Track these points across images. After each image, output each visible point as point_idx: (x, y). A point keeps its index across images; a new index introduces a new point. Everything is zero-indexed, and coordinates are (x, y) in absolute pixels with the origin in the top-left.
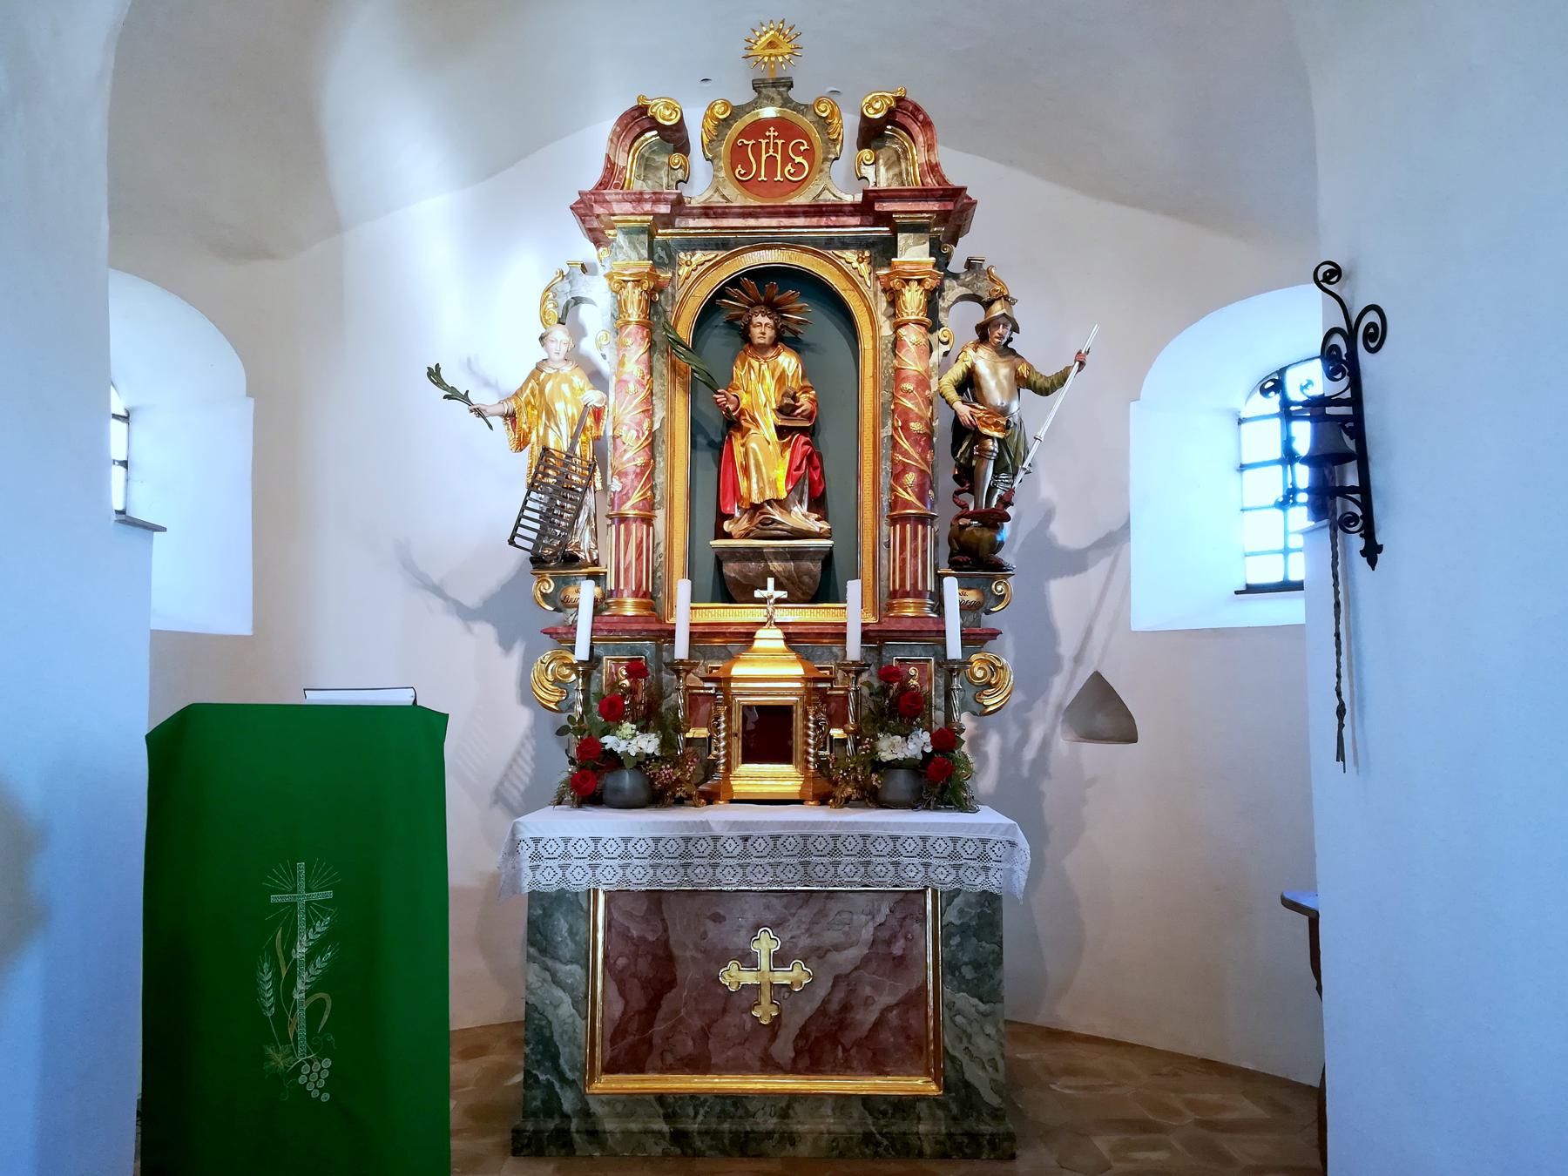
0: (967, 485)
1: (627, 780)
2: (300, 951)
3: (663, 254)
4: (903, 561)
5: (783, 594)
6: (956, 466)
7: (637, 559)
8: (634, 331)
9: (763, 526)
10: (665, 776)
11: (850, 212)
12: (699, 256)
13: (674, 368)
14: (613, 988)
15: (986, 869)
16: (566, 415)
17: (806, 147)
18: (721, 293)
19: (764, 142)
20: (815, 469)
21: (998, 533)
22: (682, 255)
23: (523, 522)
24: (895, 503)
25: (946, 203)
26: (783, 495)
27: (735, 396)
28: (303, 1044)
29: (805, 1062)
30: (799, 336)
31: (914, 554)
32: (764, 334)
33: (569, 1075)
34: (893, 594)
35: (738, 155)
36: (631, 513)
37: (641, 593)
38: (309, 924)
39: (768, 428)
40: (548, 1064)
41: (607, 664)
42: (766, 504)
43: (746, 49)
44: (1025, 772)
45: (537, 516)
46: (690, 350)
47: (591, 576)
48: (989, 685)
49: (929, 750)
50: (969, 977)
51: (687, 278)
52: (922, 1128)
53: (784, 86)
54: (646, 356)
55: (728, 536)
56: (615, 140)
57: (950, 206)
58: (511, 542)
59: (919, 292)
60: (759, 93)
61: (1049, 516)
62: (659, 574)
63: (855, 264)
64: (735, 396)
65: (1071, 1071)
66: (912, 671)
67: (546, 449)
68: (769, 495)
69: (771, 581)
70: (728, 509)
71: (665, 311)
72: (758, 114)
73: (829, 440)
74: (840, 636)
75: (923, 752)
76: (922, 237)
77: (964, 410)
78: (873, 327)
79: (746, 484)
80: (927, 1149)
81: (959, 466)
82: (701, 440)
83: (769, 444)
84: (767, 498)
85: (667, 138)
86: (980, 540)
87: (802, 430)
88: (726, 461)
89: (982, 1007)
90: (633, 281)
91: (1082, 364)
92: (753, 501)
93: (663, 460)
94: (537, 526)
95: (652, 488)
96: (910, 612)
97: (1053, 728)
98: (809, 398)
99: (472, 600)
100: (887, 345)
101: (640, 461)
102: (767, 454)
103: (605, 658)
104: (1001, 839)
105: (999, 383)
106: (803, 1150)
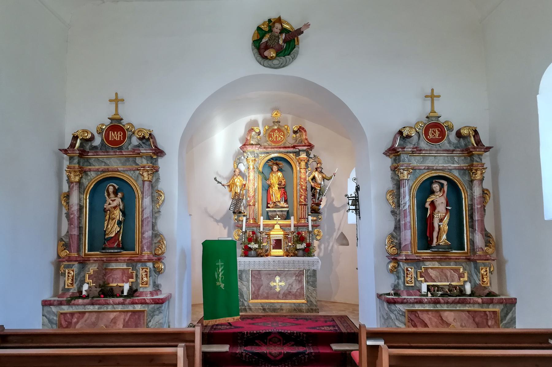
1: (253, 252)
2: (220, 271)
3: (256, 155)
4: (302, 212)
5: (280, 219)
9: (276, 206)
12: (263, 155)
14: (252, 286)
15: (314, 266)
16: (239, 185)
19: (275, 133)
24: (300, 202)
28: (221, 282)
33: (246, 300)
34: (300, 218)
35: (270, 136)
36: (252, 204)
38: (221, 267)
41: (248, 231)
44: (329, 252)
48: (318, 235)
49: (305, 247)
50: (311, 284)
55: (269, 208)
61: (333, 200)
63: (292, 156)
66: (303, 233)
67: (236, 192)
69: (277, 216)
73: (287, 189)
77: (313, 184)
78: (296, 168)
80: (304, 311)
82: (264, 189)
87: (283, 188)
89: (314, 289)
91: (334, 175)
96: (303, 222)
99: (218, 218)
101: (253, 195)
105: (319, 179)
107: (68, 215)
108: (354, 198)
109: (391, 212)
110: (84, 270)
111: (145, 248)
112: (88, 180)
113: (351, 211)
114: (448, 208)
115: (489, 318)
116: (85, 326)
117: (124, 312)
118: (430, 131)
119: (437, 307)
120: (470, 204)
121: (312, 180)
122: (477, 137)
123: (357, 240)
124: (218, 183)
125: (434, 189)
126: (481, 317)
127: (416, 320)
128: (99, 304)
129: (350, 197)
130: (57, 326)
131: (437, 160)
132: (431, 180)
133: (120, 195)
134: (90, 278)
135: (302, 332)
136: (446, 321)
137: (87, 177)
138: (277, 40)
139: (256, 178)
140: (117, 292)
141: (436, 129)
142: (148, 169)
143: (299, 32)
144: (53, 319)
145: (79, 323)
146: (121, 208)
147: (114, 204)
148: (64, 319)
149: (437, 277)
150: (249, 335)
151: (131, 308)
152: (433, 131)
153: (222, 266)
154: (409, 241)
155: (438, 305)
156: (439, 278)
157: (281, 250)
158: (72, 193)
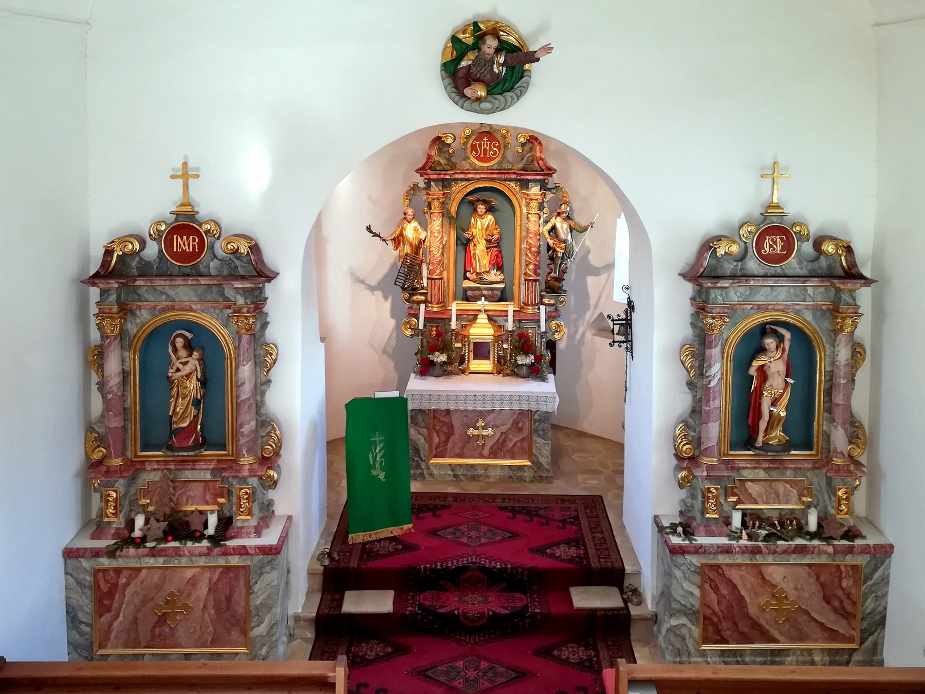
1: (437, 370)
2: (377, 450)
4: (528, 294)
24: (526, 274)
26: (488, 269)
29: (492, 455)
33: (423, 459)
40: (417, 455)
45: (403, 275)
48: (557, 331)
49: (533, 361)
52: (526, 474)
58: (395, 284)
61: (588, 252)
63: (514, 187)
65: (580, 451)
69: (483, 298)
77: (551, 242)
80: (528, 480)
82: (459, 243)
87: (495, 247)
89: (545, 442)
91: (592, 227)
96: (530, 311)
97: (586, 330)
99: (373, 283)
101: (439, 259)
105: (563, 232)
106: (491, 480)
107: (101, 386)
108: (624, 322)
109: (687, 383)
110: (136, 483)
111: (245, 452)
112: (137, 324)
113: (616, 344)
114: (789, 380)
115: (843, 575)
116: (141, 590)
117: (210, 567)
118: (767, 241)
119: (755, 558)
120: (828, 371)
121: (550, 232)
122: (851, 257)
123: (626, 390)
125: (766, 346)
126: (831, 573)
127: (718, 579)
128: (165, 556)
129: (616, 320)
130: (91, 590)
131: (775, 294)
132: (764, 330)
133: (196, 356)
134: (147, 497)
135: (522, 568)
136: (769, 581)
137: (135, 319)
138: (489, 66)
139: (446, 226)
140: (196, 525)
141: (778, 237)
142: (248, 315)
143: (532, 58)
144: (84, 579)
145: (131, 586)
146: (199, 377)
147: (187, 369)
148: (105, 580)
149: (760, 495)
150: (428, 572)
151: (221, 561)
152: (772, 240)
153: (380, 442)
154: (716, 440)
155: (758, 556)
156: (765, 496)
157: (487, 362)
158: (108, 355)
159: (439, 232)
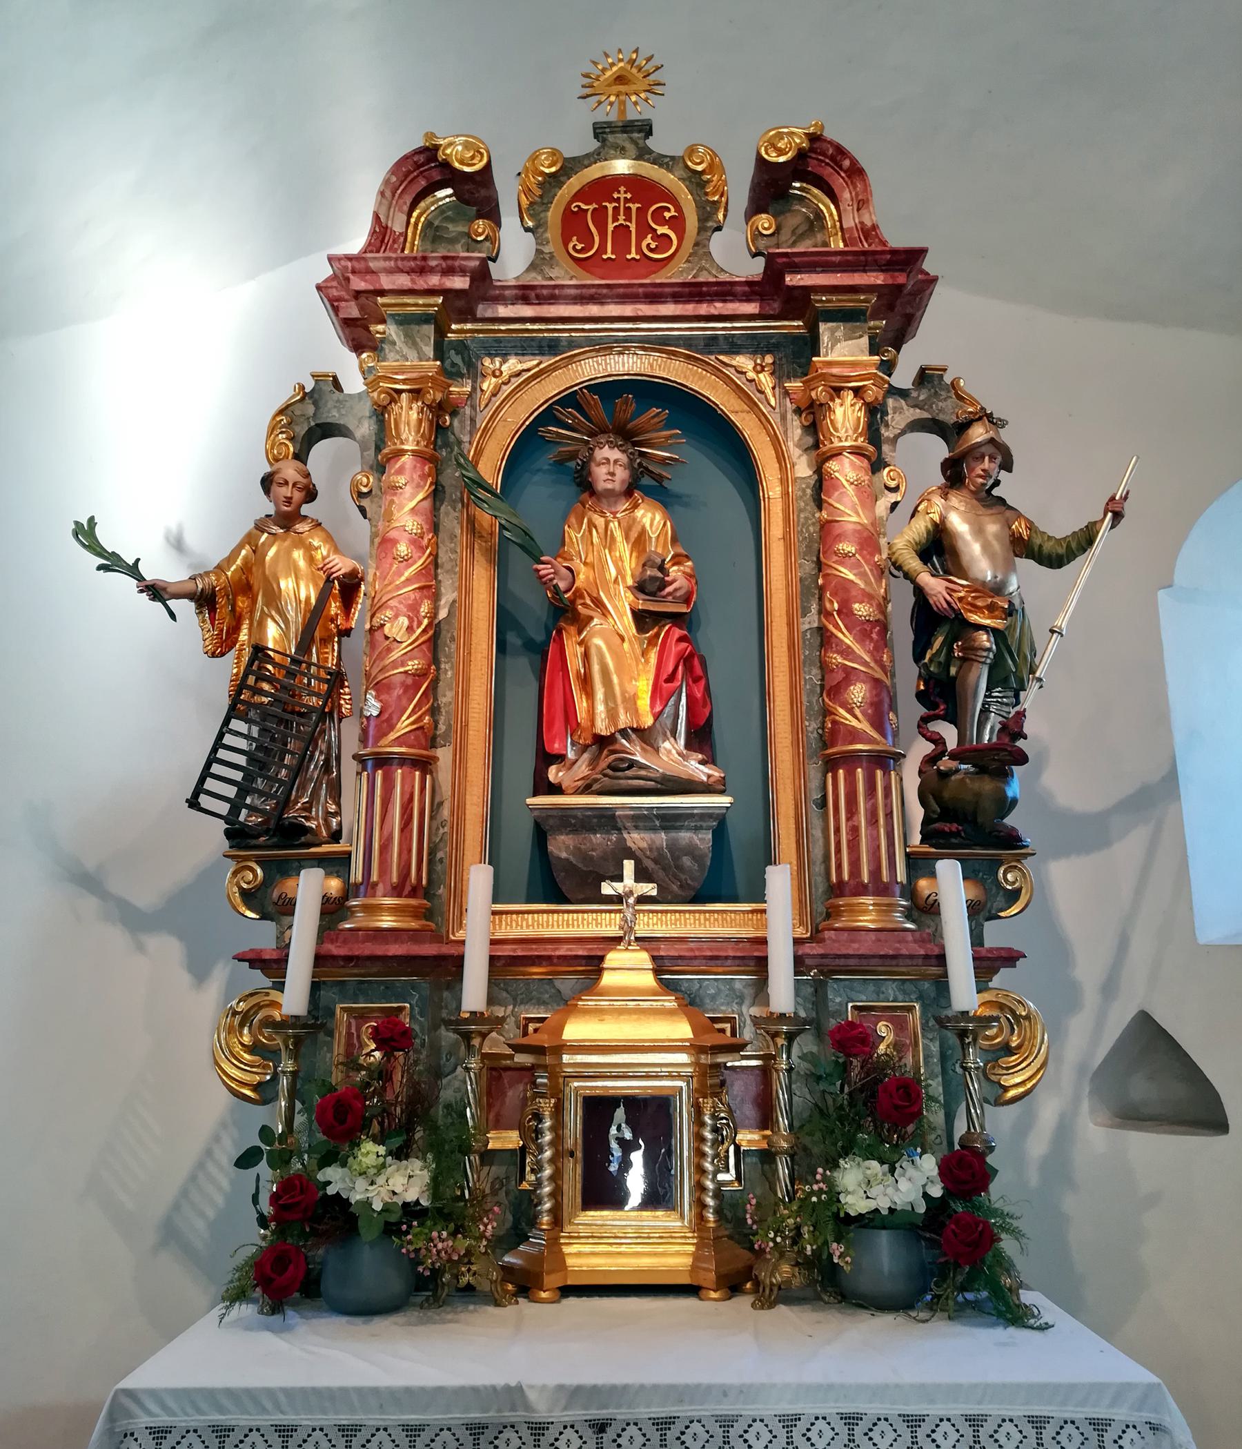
0: (942, 707)
4: (854, 830)
5: (650, 889)
6: (920, 676)
7: (402, 830)
8: (408, 466)
10: (439, 1252)
11: (744, 294)
12: (512, 364)
13: (472, 525)
17: (673, 213)
18: (548, 416)
19: (610, 206)
20: (697, 680)
21: (1007, 783)
22: (487, 361)
23: (216, 769)
24: (832, 734)
25: (896, 274)
26: (648, 721)
27: (568, 568)
30: (665, 483)
31: (873, 820)
32: (613, 474)
37: (407, 889)
39: (621, 616)
42: (618, 736)
43: (583, 86)
44: (1033, 1178)
46: (498, 497)
47: (324, 861)
49: (936, 1191)
51: (494, 395)
53: (640, 131)
54: (427, 504)
55: (556, 789)
56: (388, 194)
57: (901, 279)
58: (193, 803)
59: (857, 407)
60: (604, 141)
62: (440, 855)
64: (568, 568)
68: (624, 720)
69: (629, 866)
70: (556, 746)
71: (460, 443)
72: (602, 167)
74: (757, 963)
75: (926, 1195)
76: (856, 327)
77: (935, 586)
79: (585, 704)
81: (926, 677)
83: (623, 639)
84: (622, 726)
85: (467, 196)
86: (978, 795)
87: (676, 618)
88: (552, 671)
90: (409, 391)
91: (1118, 516)
92: (598, 731)
93: (452, 668)
94: (238, 776)
95: (434, 711)
96: (867, 920)
98: (684, 573)
99: (145, 897)
100: (804, 491)
101: (413, 665)
102: (618, 656)
103: (339, 1006)
104: (1134, 1418)
105: (986, 548)
124: (100, 568)
159: (415, 542)
